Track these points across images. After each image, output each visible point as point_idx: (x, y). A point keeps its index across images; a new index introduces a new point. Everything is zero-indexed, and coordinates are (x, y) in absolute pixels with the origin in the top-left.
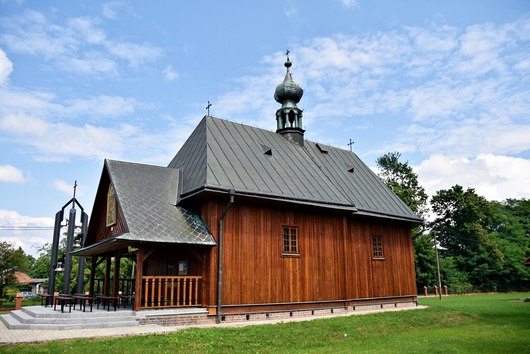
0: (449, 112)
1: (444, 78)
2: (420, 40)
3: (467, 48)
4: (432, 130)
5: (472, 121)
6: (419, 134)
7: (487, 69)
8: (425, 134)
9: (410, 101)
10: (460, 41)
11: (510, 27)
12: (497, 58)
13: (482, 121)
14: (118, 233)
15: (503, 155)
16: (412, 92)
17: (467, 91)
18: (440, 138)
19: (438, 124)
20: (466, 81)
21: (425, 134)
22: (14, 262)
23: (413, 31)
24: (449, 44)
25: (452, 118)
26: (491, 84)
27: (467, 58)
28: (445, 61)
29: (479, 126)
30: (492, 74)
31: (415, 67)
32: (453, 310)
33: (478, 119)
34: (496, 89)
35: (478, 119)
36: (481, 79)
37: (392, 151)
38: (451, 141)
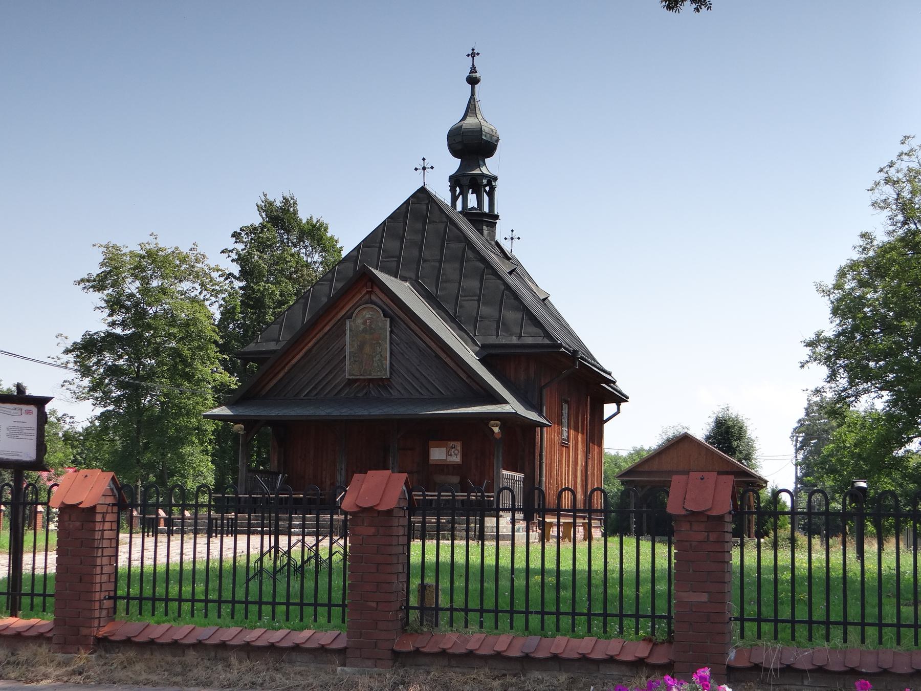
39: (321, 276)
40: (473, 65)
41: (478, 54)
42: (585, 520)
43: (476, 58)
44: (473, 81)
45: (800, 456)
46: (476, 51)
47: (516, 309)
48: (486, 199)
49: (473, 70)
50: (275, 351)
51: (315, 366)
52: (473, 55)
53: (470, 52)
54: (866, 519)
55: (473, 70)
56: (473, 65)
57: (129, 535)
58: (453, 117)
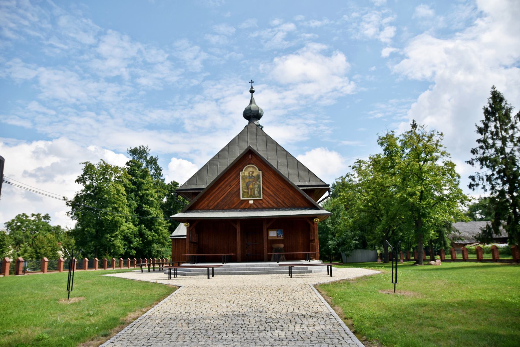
0: (73, 101)
1: (77, 67)
2: (63, 21)
3: (104, 49)
4: (53, 112)
5: (93, 114)
6: (38, 113)
7: (116, 73)
8: (45, 114)
9: (37, 77)
10: (99, 40)
11: (139, 46)
12: (126, 68)
13: (101, 118)
14: (329, 267)
15: (110, 150)
16: (42, 69)
17: (93, 86)
18: (60, 121)
19: (60, 108)
20: (96, 78)
21: (45, 114)
22: (57, 323)
23: (58, 11)
24: (88, 39)
25: (75, 106)
26: (113, 88)
27: (99, 57)
28: (81, 52)
29: (98, 121)
30: (118, 80)
31: (51, 46)
32: (157, 300)
33: (98, 114)
34: (119, 93)
35: (98, 114)
36: (109, 80)
37: (145, 145)
38: (71, 128)
39: (165, 200)
40: (252, 86)
41: (254, 82)
42: (314, 271)
43: (253, 83)
44: (252, 92)
45: (442, 233)
46: (253, 81)
47: (290, 156)
48: (72, 271)
49: (252, 87)
50: (203, 189)
51: (223, 189)
52: (252, 82)
53: (250, 81)
54: (135, 254)
55: (252, 87)
56: (252, 86)
57: (207, 276)
58: (246, 104)
